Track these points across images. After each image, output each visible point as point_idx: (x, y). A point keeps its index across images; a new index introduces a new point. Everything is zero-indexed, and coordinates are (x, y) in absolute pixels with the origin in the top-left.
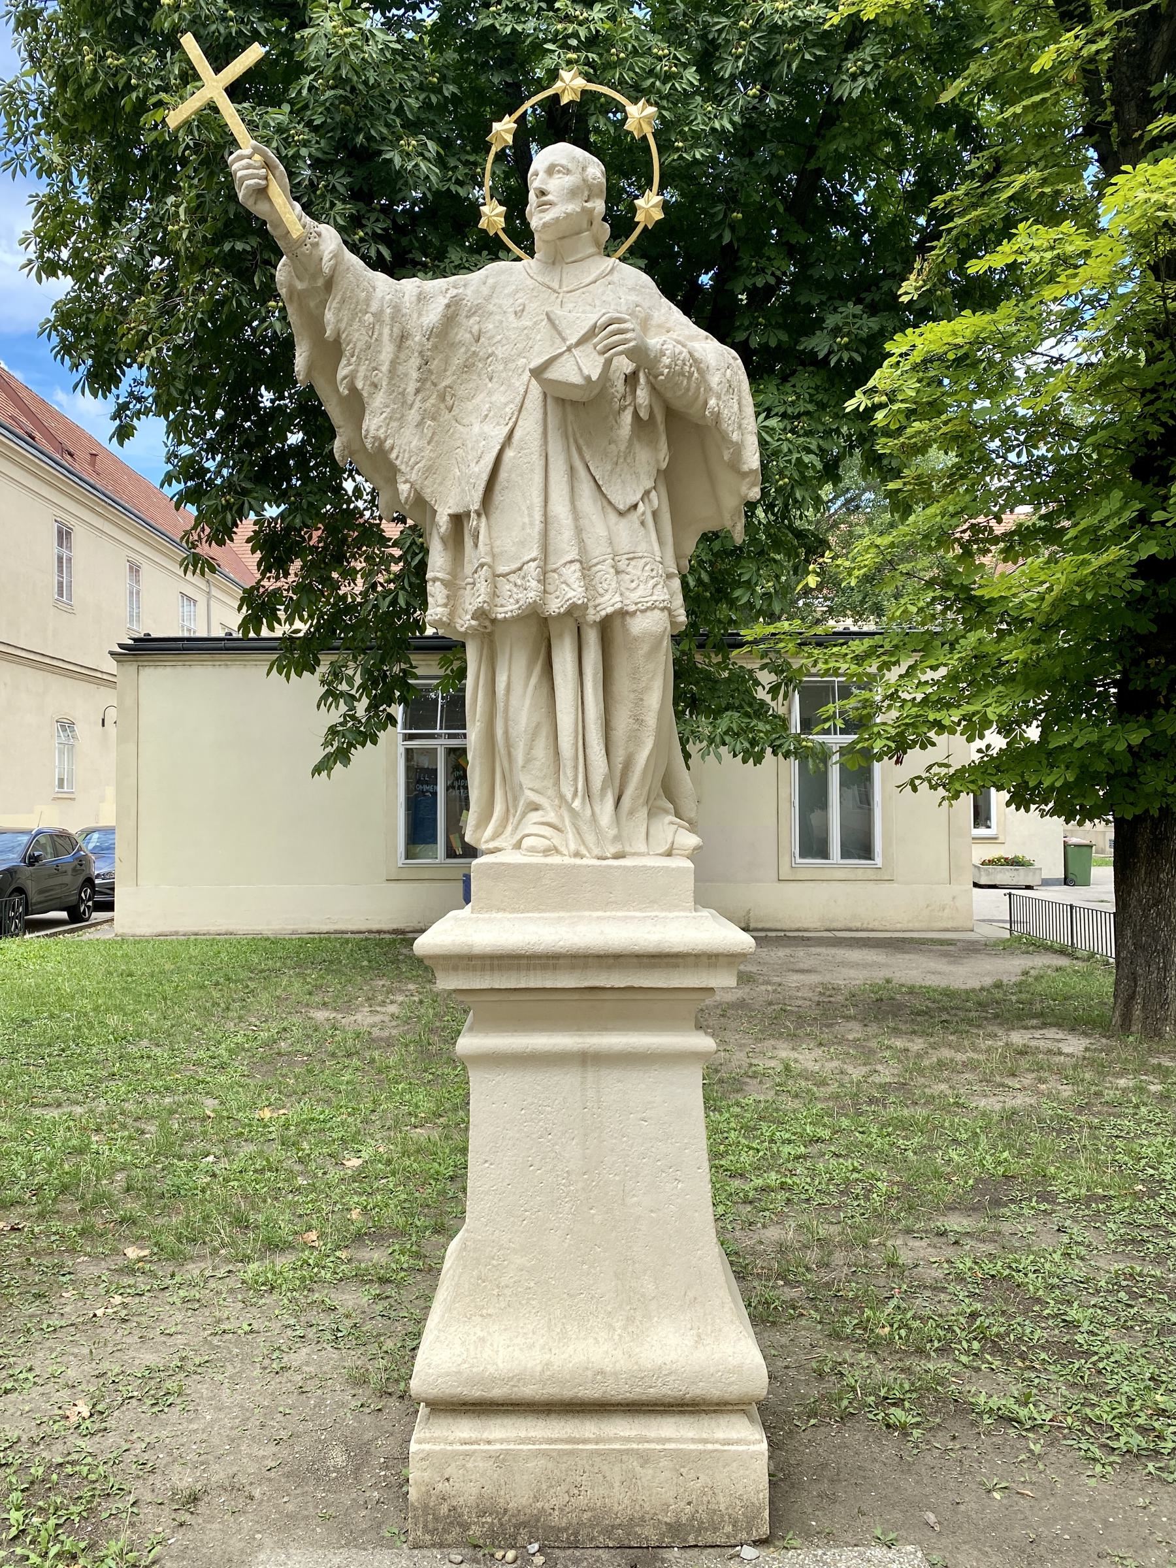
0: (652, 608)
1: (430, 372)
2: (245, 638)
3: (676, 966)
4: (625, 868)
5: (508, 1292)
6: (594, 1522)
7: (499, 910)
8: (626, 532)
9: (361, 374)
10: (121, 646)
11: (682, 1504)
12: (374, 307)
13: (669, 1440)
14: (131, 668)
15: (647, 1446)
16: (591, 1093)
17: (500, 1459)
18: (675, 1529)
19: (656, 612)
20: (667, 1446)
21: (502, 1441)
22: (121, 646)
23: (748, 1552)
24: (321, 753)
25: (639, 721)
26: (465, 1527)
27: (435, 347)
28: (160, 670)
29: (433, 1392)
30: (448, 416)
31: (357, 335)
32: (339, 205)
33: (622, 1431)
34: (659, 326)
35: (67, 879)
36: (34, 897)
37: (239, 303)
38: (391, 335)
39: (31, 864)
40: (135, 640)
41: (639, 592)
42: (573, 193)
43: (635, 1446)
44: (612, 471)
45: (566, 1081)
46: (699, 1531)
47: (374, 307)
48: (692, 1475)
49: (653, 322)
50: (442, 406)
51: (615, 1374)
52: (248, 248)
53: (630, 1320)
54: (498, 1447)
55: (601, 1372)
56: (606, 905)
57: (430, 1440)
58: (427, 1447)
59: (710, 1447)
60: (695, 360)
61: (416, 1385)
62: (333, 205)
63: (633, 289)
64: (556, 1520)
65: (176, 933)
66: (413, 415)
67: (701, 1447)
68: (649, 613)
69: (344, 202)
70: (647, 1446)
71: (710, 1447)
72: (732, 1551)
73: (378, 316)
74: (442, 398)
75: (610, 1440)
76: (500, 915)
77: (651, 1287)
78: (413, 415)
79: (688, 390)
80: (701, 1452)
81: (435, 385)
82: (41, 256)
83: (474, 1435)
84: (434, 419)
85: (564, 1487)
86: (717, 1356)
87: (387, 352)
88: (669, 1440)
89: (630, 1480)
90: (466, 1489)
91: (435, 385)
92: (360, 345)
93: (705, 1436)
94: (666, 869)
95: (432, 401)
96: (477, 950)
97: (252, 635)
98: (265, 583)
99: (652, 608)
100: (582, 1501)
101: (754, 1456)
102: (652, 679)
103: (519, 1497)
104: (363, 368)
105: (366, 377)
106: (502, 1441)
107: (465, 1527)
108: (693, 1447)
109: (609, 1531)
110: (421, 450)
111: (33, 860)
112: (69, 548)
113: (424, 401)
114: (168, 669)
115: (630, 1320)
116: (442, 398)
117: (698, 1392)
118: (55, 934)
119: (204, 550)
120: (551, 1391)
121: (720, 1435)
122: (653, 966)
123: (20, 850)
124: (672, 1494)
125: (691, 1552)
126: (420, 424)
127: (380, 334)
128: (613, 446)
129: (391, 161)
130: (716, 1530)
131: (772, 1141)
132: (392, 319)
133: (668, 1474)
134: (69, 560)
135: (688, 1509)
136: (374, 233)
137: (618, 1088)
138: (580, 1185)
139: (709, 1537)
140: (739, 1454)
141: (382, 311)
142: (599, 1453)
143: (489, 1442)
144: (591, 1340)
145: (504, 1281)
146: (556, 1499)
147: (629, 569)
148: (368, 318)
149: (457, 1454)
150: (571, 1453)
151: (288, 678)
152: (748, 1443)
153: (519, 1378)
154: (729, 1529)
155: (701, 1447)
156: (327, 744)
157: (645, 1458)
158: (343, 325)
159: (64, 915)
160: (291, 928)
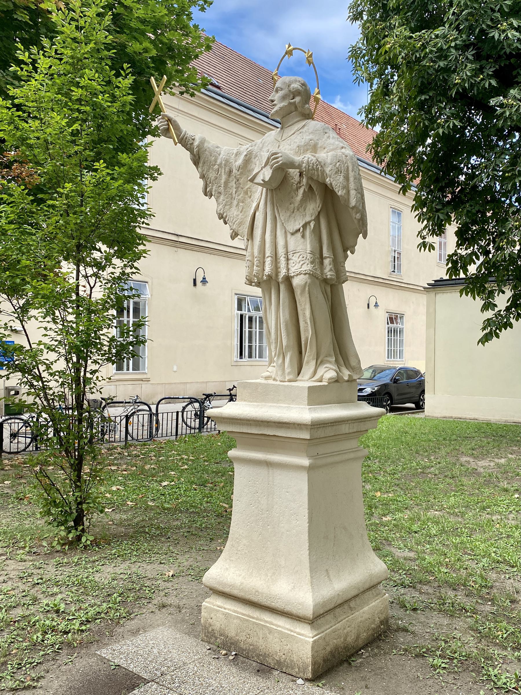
0: (300, 274)
1: (240, 184)
2: (450, 279)
3: (289, 428)
4: (284, 386)
5: (239, 553)
6: (254, 650)
7: (245, 401)
8: (294, 242)
9: (214, 190)
10: (428, 284)
11: (282, 654)
12: (219, 162)
13: (279, 626)
14: (432, 294)
15: (272, 626)
16: (271, 478)
17: (226, 615)
18: (279, 662)
19: (302, 275)
20: (279, 629)
21: (229, 609)
22: (428, 284)
23: (300, 681)
24: (482, 334)
25: (306, 323)
26: (216, 638)
27: (242, 173)
28: (445, 295)
29: (208, 584)
30: (249, 200)
31: (211, 175)
32: (469, 65)
33: (267, 618)
34: (321, 147)
35: (413, 390)
36: (395, 397)
37: (424, 124)
38: (225, 172)
39: (395, 382)
40: (435, 281)
41: (296, 267)
42: (284, 98)
43: (268, 625)
44: (290, 216)
45: (263, 471)
46: (287, 667)
47: (219, 162)
48: (285, 643)
49: (319, 146)
50: (247, 196)
51: (262, 593)
52: (428, 97)
53: (274, 574)
54: (227, 611)
55: (257, 591)
56: (278, 401)
57: (212, 603)
58: (207, 604)
59: (292, 633)
60: (320, 163)
61: (204, 579)
62: (466, 66)
63: (312, 133)
64: (242, 645)
65: (451, 417)
66: (235, 202)
67: (289, 632)
68: (298, 276)
69: (472, 63)
70: (272, 626)
71: (292, 633)
72: (295, 679)
73: (220, 165)
74: (246, 193)
75: (261, 620)
76: (245, 403)
77: (283, 562)
78: (235, 202)
79: (318, 175)
80: (289, 634)
81: (242, 188)
82: (367, 117)
83: (222, 605)
84: (243, 202)
85: (244, 634)
86: (297, 596)
87: (224, 177)
88: (279, 626)
89: (265, 638)
90: (217, 623)
91: (242, 188)
92: (213, 178)
93: (292, 629)
94: (282, 385)
95: (241, 195)
96: (224, 416)
97: (454, 277)
98: (459, 251)
99: (300, 274)
100: (250, 641)
101: (307, 642)
102: (305, 305)
103: (232, 633)
104: (214, 187)
105: (215, 190)
106: (229, 609)
107: (216, 638)
108: (286, 631)
109: (258, 656)
110: (238, 216)
111: (395, 381)
112: (445, 238)
113: (238, 196)
114: (449, 294)
115: (274, 574)
116: (246, 193)
117: (288, 609)
118: (402, 414)
119: (430, 239)
120: (241, 594)
121: (298, 630)
122: (281, 427)
123: (390, 376)
124: (278, 648)
125: (283, 675)
126: (237, 205)
127: (221, 172)
128: (292, 205)
129: (493, 37)
130: (292, 669)
131: (508, 536)
132: (225, 165)
133: (277, 640)
134: (445, 243)
135: (284, 656)
136: (488, 75)
137: (280, 478)
138: (266, 515)
139: (289, 671)
140: (302, 640)
141: (221, 163)
142: (258, 624)
143: (225, 609)
144: (259, 578)
145: (239, 548)
146: (242, 637)
147: (293, 258)
148: (216, 167)
149: (214, 610)
150: (247, 620)
151: (474, 298)
152: (306, 637)
153: (232, 586)
154: (297, 670)
155: (289, 632)
156: (484, 329)
157: (270, 631)
158: (205, 172)
159: (413, 405)
160: (504, 419)
